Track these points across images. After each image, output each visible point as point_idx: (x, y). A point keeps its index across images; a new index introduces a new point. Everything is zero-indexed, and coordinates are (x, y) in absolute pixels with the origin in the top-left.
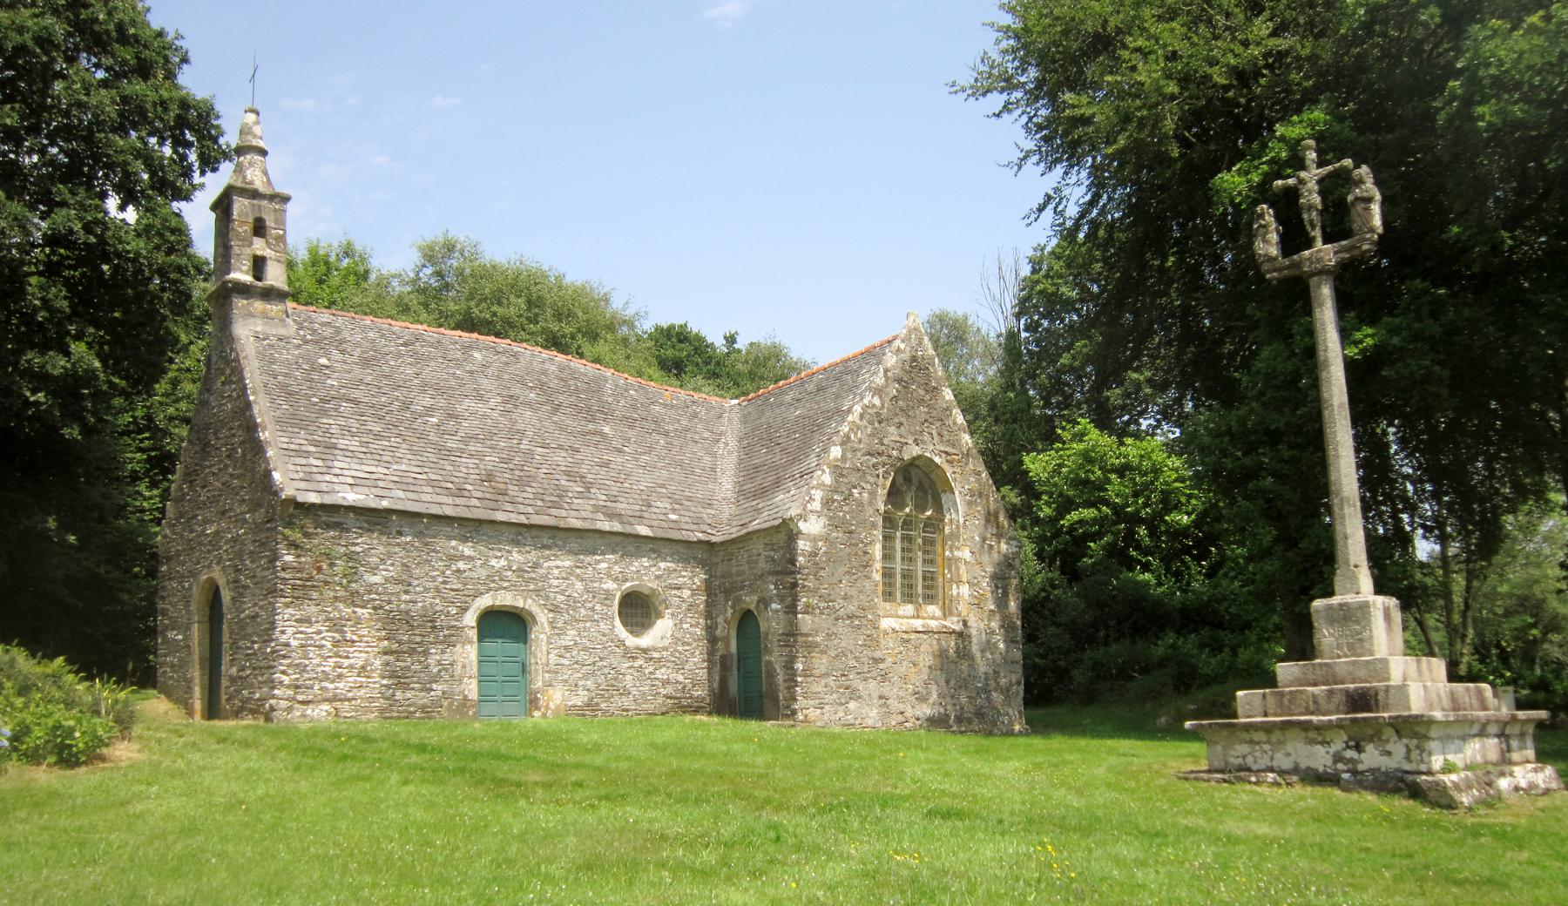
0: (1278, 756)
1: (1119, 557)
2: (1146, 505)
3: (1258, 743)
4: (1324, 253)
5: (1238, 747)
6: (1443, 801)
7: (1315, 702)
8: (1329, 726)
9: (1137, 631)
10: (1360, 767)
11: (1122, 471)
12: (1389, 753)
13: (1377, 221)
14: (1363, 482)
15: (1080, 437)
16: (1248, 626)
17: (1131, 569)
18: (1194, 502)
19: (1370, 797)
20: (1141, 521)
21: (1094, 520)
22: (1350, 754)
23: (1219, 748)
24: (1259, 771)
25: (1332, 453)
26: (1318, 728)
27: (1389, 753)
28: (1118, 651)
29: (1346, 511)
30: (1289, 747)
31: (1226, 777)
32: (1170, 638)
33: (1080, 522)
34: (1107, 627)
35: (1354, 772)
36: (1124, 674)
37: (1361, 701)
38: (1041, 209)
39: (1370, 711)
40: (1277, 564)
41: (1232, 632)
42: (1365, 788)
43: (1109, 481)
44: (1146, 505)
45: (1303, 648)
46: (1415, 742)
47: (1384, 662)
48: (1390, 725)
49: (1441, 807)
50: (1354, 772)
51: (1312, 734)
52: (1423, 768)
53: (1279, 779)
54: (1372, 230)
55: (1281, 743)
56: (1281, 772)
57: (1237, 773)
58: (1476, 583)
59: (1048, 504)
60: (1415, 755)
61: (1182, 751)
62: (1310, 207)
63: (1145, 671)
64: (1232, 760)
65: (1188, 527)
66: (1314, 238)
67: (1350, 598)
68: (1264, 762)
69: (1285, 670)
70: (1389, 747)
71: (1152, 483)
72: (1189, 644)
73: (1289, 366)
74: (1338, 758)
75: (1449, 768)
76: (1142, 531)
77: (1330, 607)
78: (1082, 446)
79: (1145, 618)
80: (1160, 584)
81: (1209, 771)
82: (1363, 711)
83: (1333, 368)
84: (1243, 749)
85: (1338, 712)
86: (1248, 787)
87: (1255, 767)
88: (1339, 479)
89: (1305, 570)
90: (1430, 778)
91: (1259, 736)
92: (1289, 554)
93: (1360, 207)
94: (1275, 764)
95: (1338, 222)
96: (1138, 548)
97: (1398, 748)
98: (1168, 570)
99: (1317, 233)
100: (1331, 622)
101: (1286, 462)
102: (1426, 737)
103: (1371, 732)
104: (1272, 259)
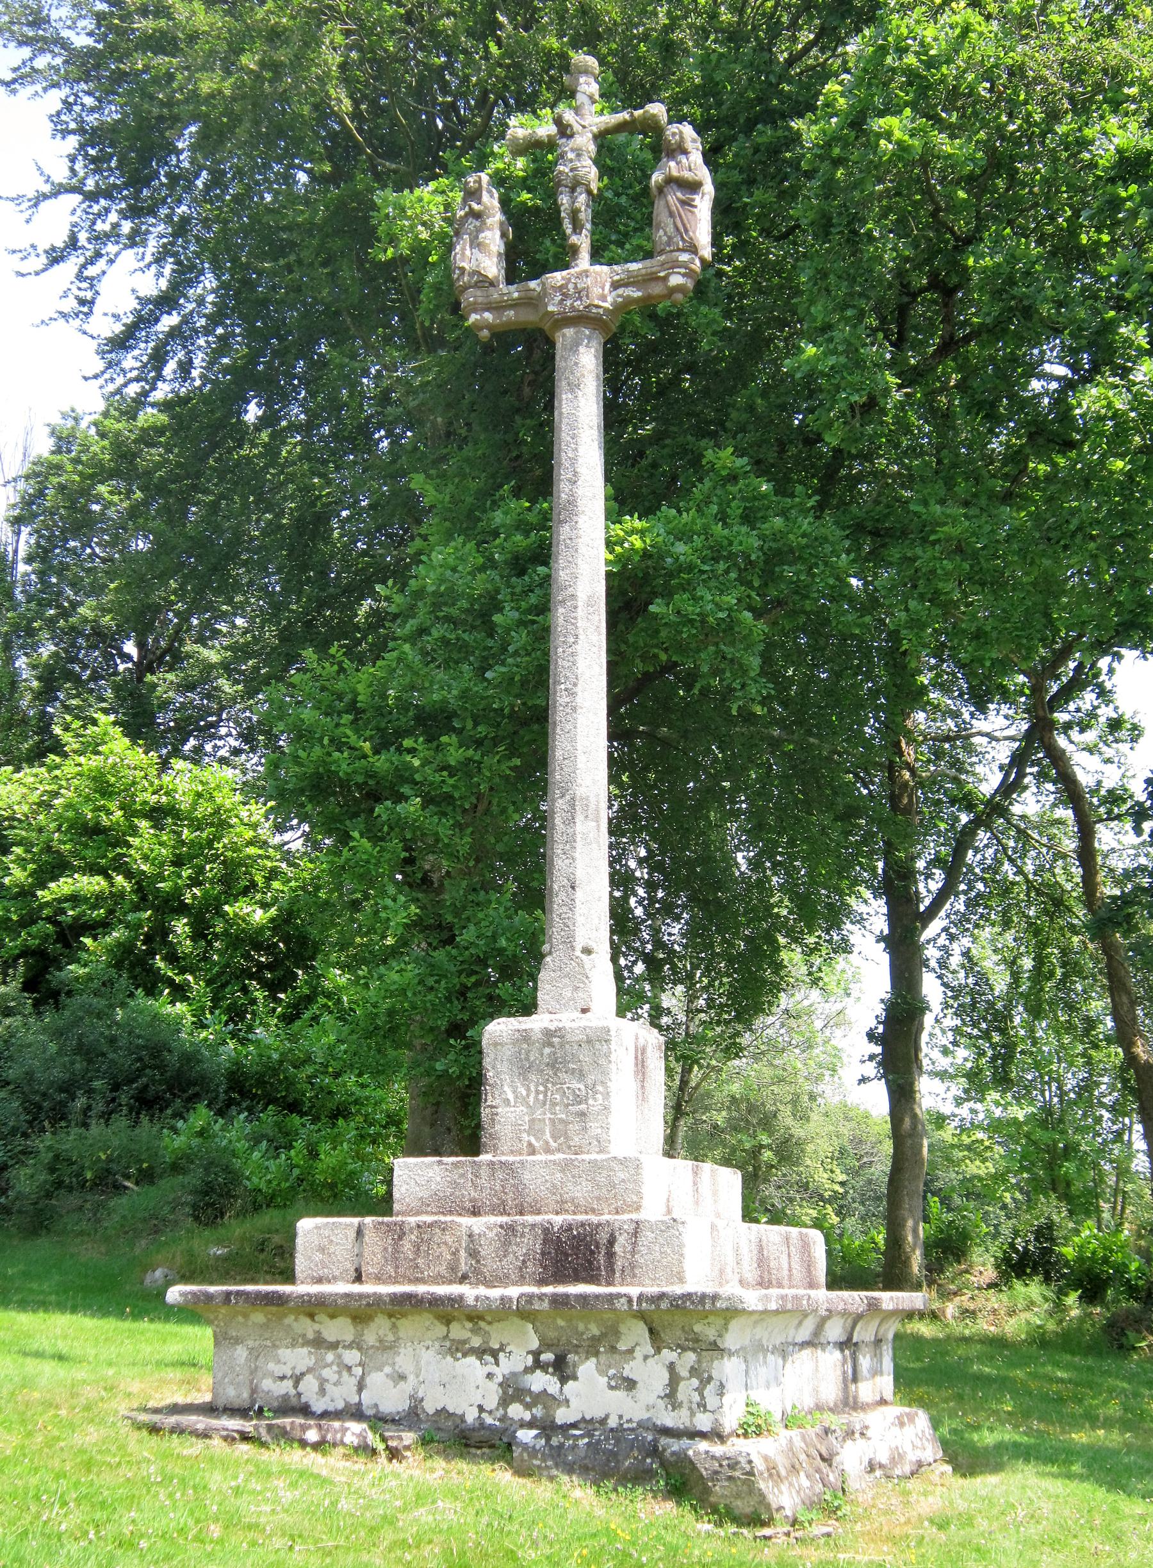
0: (377, 1380)
1: (137, 969)
2: (195, 882)
3: (334, 1346)
4: (593, 282)
5: (285, 1353)
6: (743, 1506)
7: (474, 1254)
8: (504, 1311)
9: (147, 1104)
10: (562, 1416)
11: (158, 815)
12: (630, 1384)
13: (702, 232)
14: (616, 765)
15: (93, 747)
16: (340, 1112)
17: (151, 992)
18: (276, 885)
19: (579, 1494)
20: (183, 909)
21: (98, 900)
22: (541, 1381)
23: (241, 1353)
24: (325, 1415)
25: (562, 699)
26: (476, 1317)
27: (630, 1384)
28: (101, 1139)
29: (580, 827)
30: (404, 1360)
31: (248, 1426)
32: (201, 1116)
33: (74, 899)
34: (90, 1092)
35: (547, 1428)
36: (107, 1182)
37: (576, 1254)
38: (56, 257)
39: (593, 1279)
40: (412, 971)
41: (316, 1119)
42: (570, 1469)
43: (134, 831)
44: (195, 882)
45: (455, 1118)
46: (691, 1357)
47: (633, 1165)
48: (641, 1316)
49: (738, 1521)
50: (547, 1428)
51: (459, 1331)
52: (703, 1422)
53: (373, 1439)
54: (693, 249)
55: (387, 1347)
56: (379, 1421)
57: (271, 1417)
58: (696, 1073)
59: (21, 862)
60: (687, 1389)
61: (174, 1350)
62: (575, 185)
63: (147, 1177)
64: (267, 1384)
65: (261, 929)
66: (575, 250)
67: (568, 1020)
68: (341, 1394)
69: (415, 1176)
70: (631, 1369)
71: (210, 844)
72: (234, 1132)
73: (481, 584)
74: (512, 1391)
75: (753, 1428)
76: (181, 926)
77: (525, 1037)
78: (95, 762)
79: (162, 1083)
80: (201, 1025)
81: (210, 1409)
82: (577, 1279)
83: (583, 521)
84: (298, 1358)
85: (522, 1280)
86: (296, 1457)
87: (318, 1406)
88: (571, 757)
89: (463, 993)
90: (718, 1449)
91: (338, 1329)
92: (440, 955)
93: (674, 197)
94: (367, 1398)
95: (626, 219)
96: (172, 958)
97: (650, 1372)
98: (216, 1001)
99: (583, 241)
100: (524, 1069)
101: (452, 771)
102: (716, 1348)
103: (595, 1330)
104: (485, 283)
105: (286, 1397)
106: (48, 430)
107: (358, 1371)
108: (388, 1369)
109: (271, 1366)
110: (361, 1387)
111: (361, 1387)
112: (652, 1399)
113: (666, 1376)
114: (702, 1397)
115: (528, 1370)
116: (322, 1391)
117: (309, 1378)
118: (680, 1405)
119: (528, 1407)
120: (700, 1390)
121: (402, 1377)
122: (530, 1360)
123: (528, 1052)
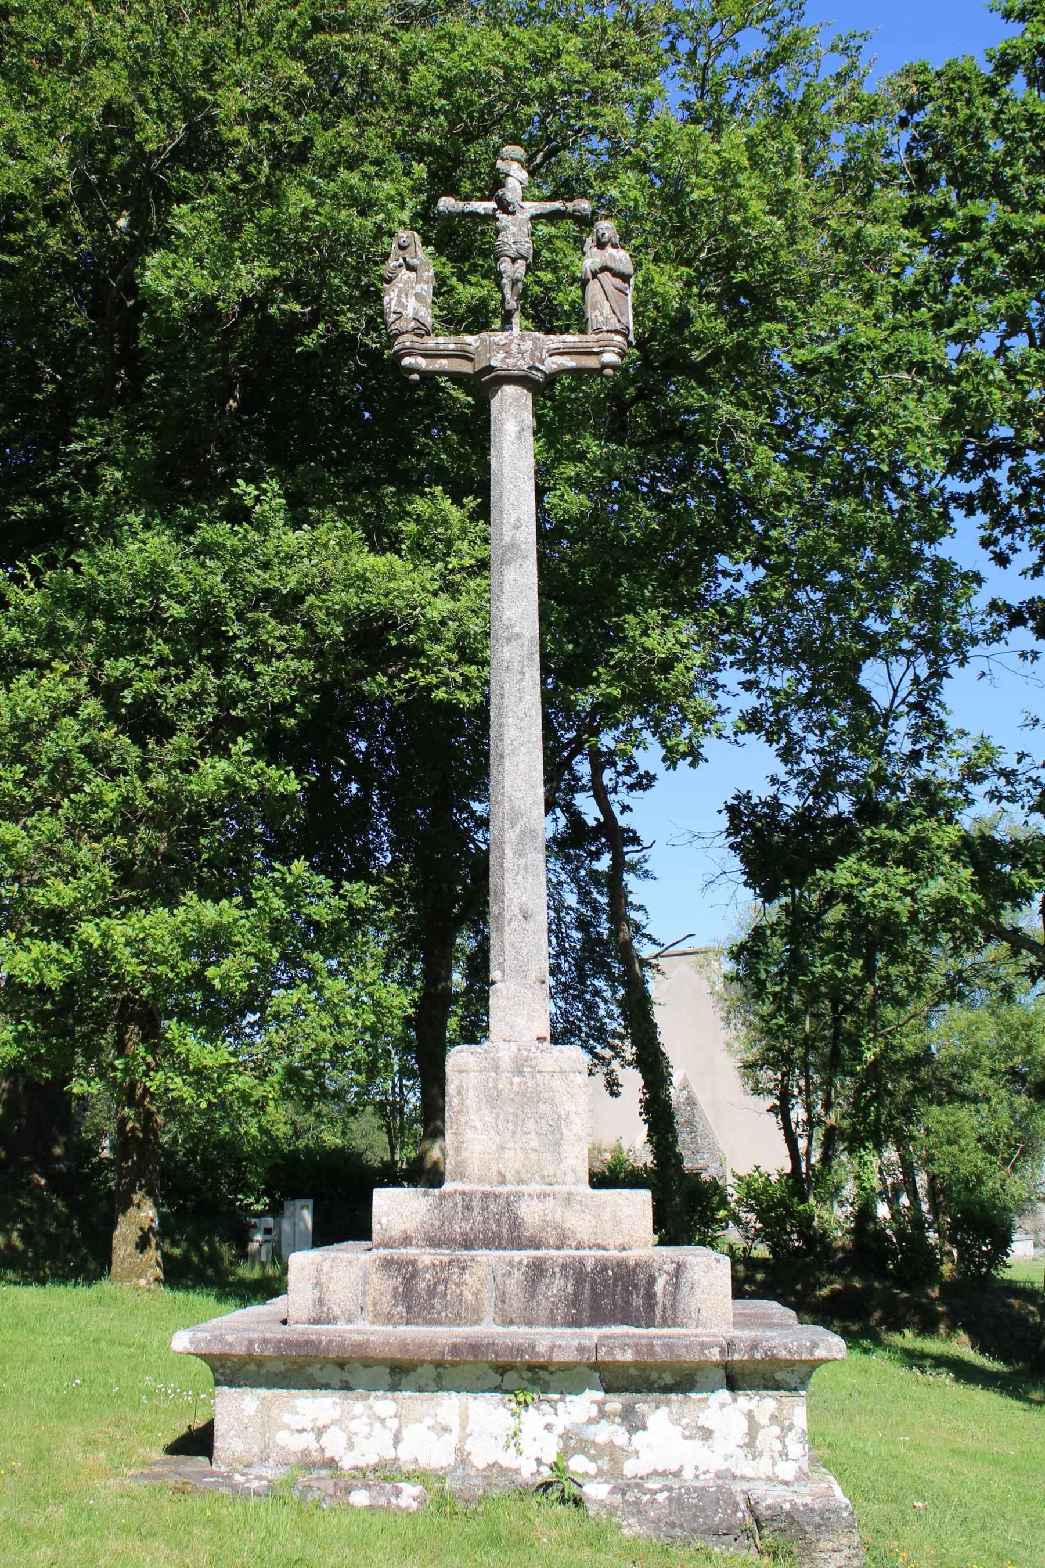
10: (630, 1468)
12: (707, 1434)
64: (283, 1438)
94: (405, 1454)
105: (306, 1453)
106: (997, 683)
107: (394, 1424)
108: (429, 1421)
109: (287, 1418)
110: (397, 1440)
111: (397, 1440)
112: (731, 1448)
113: (745, 1424)
114: (785, 1446)
115: (591, 1421)
116: (351, 1446)
117: (333, 1430)
118: (761, 1455)
119: (593, 1459)
120: (782, 1438)
121: (446, 1429)
122: (594, 1411)
123: (496, 1081)
